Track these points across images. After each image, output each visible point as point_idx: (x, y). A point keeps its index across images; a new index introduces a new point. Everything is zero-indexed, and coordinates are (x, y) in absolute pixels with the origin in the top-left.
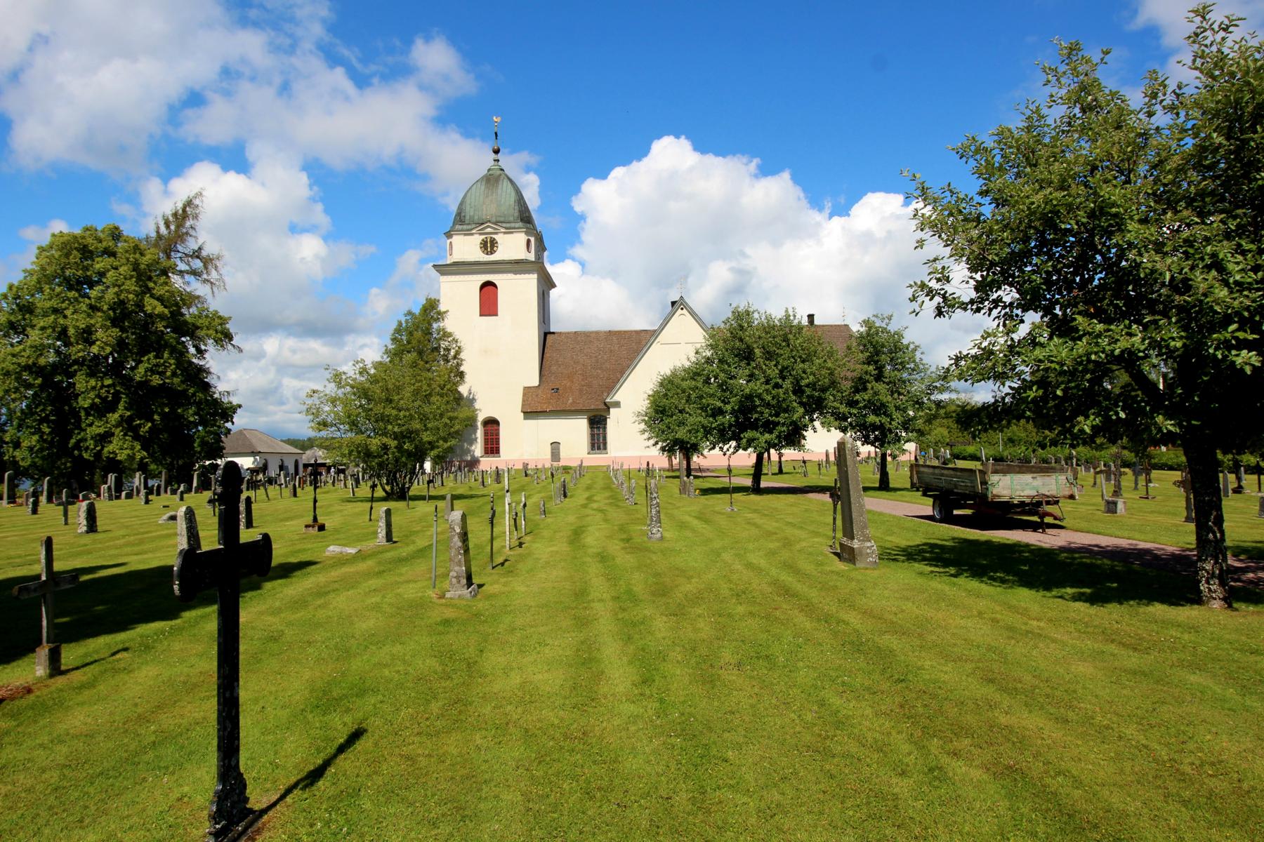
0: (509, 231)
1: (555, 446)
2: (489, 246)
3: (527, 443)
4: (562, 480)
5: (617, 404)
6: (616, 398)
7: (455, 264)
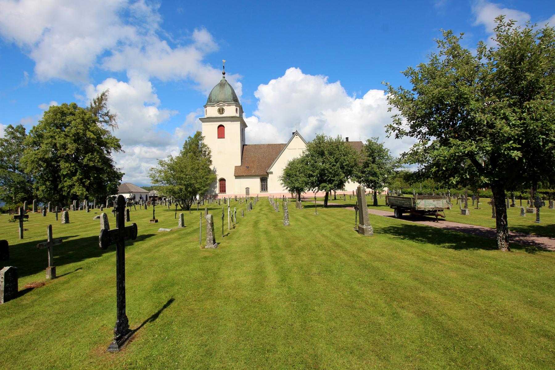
0: (229, 105)
1: (247, 189)
2: (221, 111)
3: (236, 188)
4: (250, 203)
5: (271, 173)
6: (271, 170)
7: (208, 118)
